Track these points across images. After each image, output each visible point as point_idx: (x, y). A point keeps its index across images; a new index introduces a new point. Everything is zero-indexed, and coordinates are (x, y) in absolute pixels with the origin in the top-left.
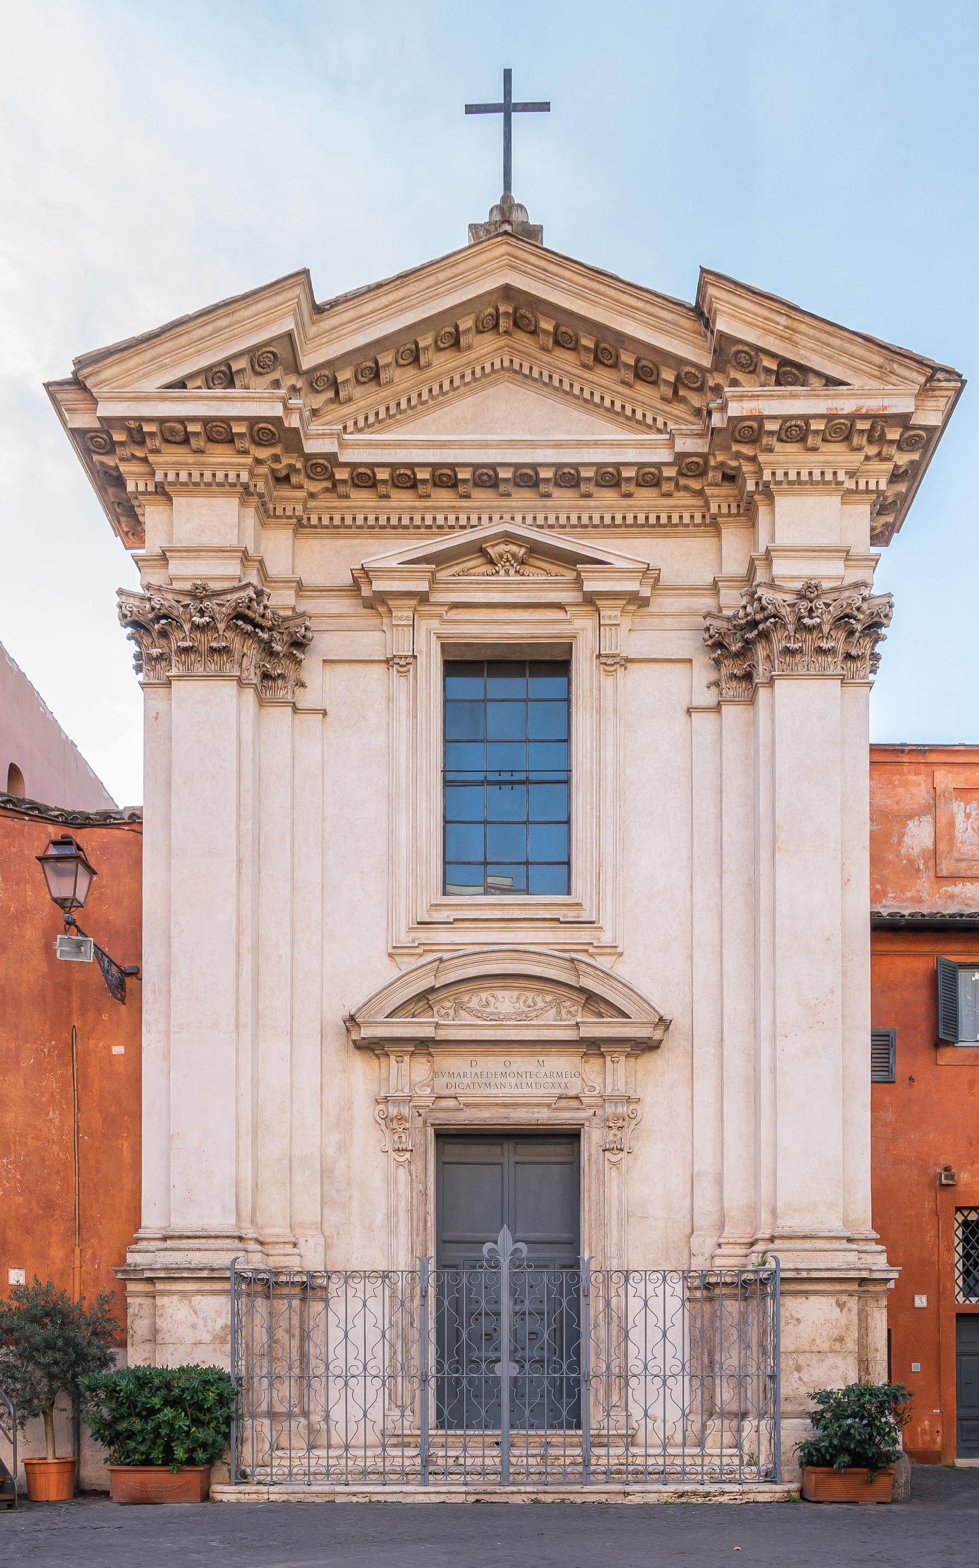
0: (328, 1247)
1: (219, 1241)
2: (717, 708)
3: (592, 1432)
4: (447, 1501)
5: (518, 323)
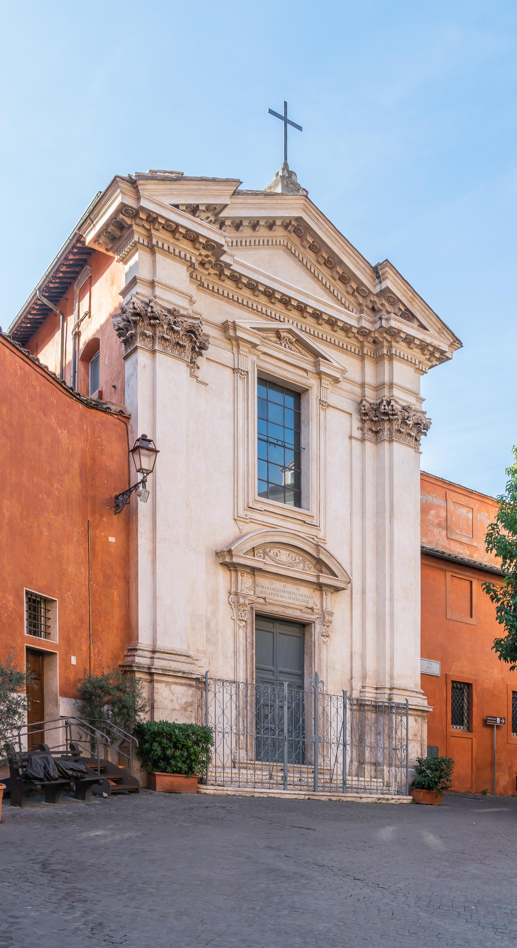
1: (180, 657)
2: (363, 440)
3: (319, 767)
4: (298, 798)
5: (296, 231)
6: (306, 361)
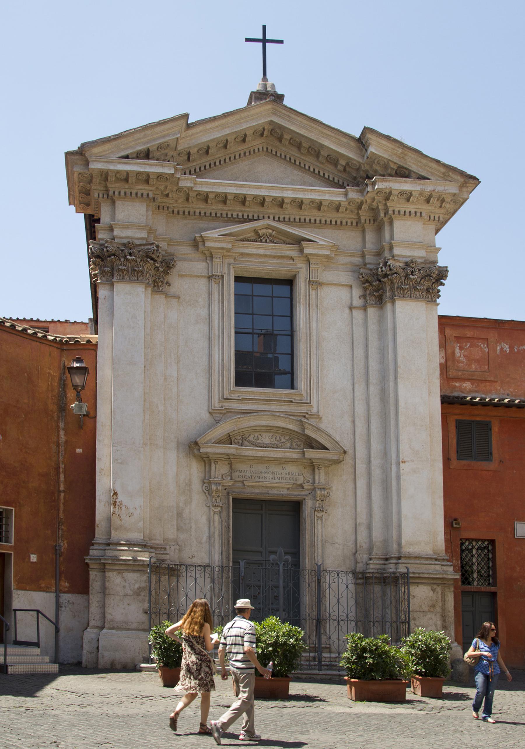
0: (180, 551)
2: (364, 308)
3: (323, 646)
6: (290, 251)
